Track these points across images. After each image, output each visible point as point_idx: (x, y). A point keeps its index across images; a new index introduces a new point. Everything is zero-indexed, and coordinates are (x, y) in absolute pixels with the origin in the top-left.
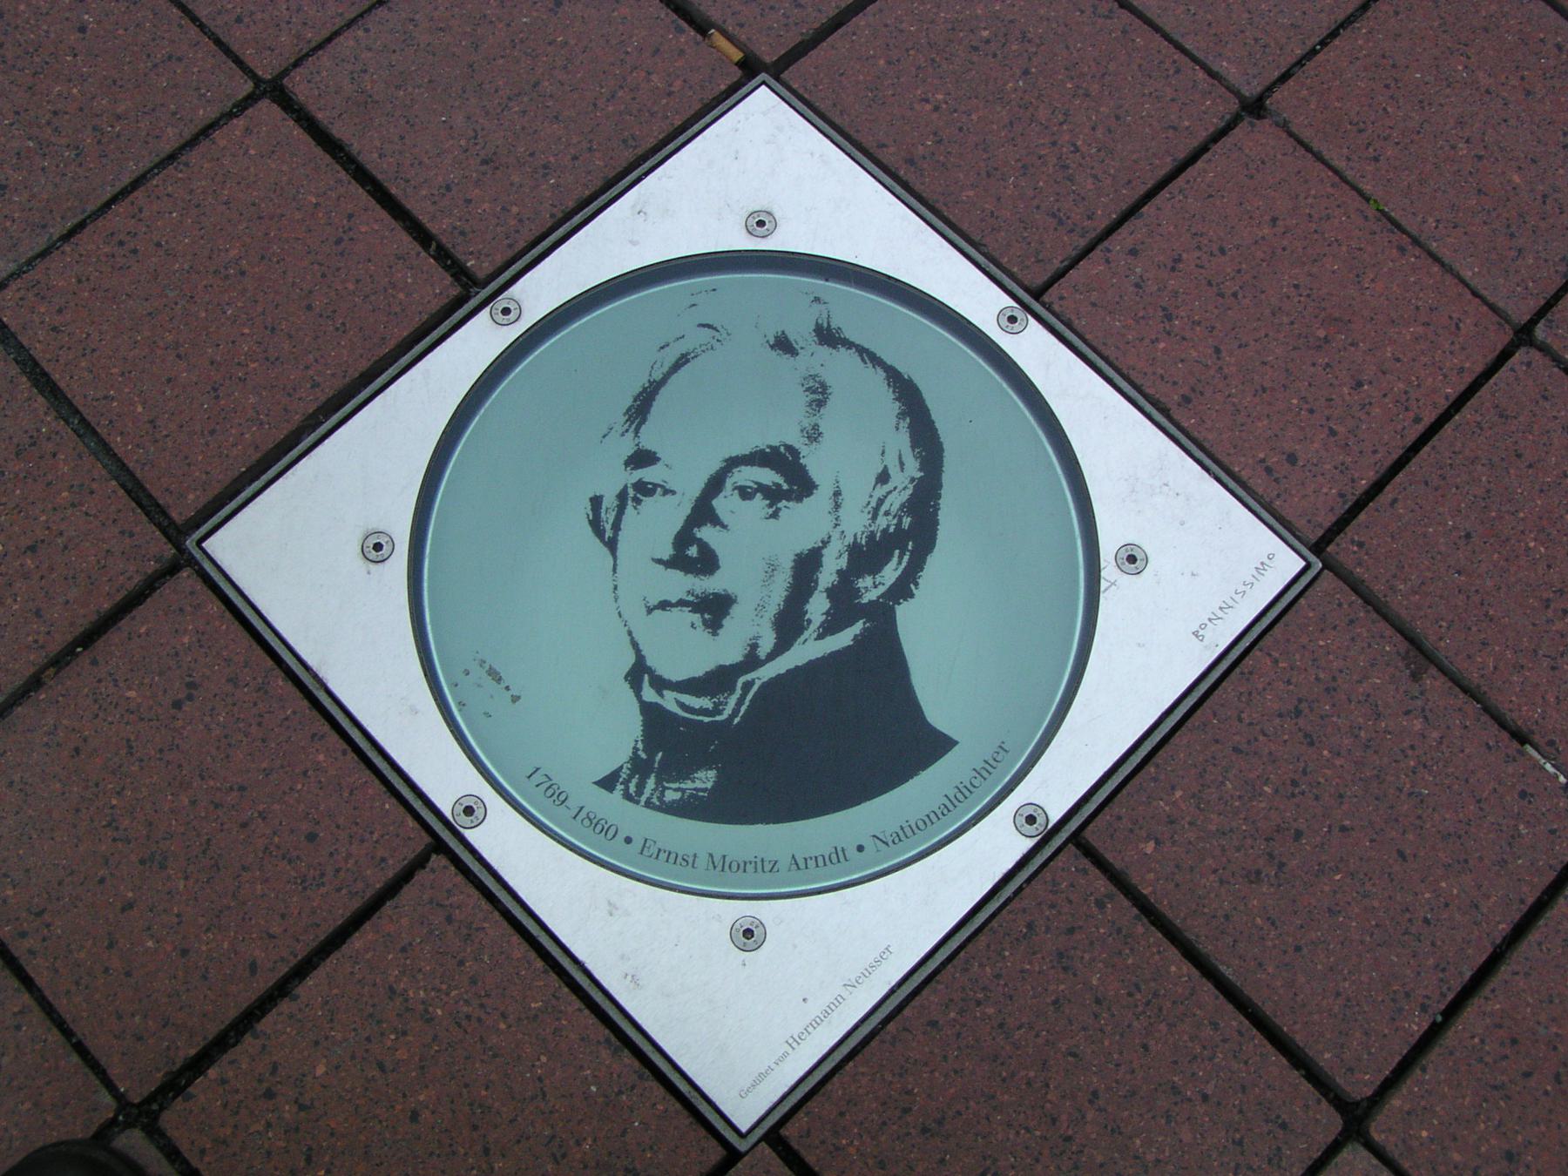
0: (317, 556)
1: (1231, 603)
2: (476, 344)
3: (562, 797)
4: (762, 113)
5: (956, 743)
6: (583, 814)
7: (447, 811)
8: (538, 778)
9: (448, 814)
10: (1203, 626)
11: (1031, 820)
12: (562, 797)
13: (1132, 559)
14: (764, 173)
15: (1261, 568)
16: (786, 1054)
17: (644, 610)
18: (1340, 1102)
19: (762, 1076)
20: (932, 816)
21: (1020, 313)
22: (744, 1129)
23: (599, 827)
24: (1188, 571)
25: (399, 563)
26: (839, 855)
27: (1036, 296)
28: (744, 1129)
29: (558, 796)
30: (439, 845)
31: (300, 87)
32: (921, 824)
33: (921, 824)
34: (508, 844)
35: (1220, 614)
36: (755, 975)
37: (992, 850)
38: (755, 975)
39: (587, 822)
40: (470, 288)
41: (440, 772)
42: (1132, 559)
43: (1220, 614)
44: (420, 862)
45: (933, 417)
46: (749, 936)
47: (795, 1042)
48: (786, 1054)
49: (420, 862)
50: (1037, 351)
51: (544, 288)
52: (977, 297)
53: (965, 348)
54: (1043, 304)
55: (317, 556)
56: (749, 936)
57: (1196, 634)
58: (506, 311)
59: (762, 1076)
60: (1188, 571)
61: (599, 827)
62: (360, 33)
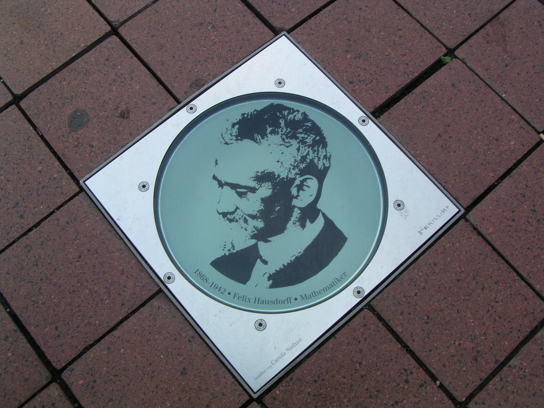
0: (123, 187)
1: (432, 222)
2: (182, 118)
15: (444, 211)
19: (262, 373)
23: (202, 278)
24: (416, 208)
26: (289, 300)
28: (255, 391)
30: (160, 292)
32: (281, 302)
33: (281, 302)
34: (180, 288)
35: (428, 226)
36: (260, 339)
37: (344, 302)
38: (260, 339)
39: (199, 275)
40: (178, 102)
41: (160, 263)
42: (261, 325)
43: (428, 226)
47: (283, 355)
48: (271, 366)
50: (372, 132)
53: (375, 168)
55: (123, 187)
57: (420, 232)
58: (191, 108)
60: (416, 208)
61: (202, 278)
62: (528, 330)
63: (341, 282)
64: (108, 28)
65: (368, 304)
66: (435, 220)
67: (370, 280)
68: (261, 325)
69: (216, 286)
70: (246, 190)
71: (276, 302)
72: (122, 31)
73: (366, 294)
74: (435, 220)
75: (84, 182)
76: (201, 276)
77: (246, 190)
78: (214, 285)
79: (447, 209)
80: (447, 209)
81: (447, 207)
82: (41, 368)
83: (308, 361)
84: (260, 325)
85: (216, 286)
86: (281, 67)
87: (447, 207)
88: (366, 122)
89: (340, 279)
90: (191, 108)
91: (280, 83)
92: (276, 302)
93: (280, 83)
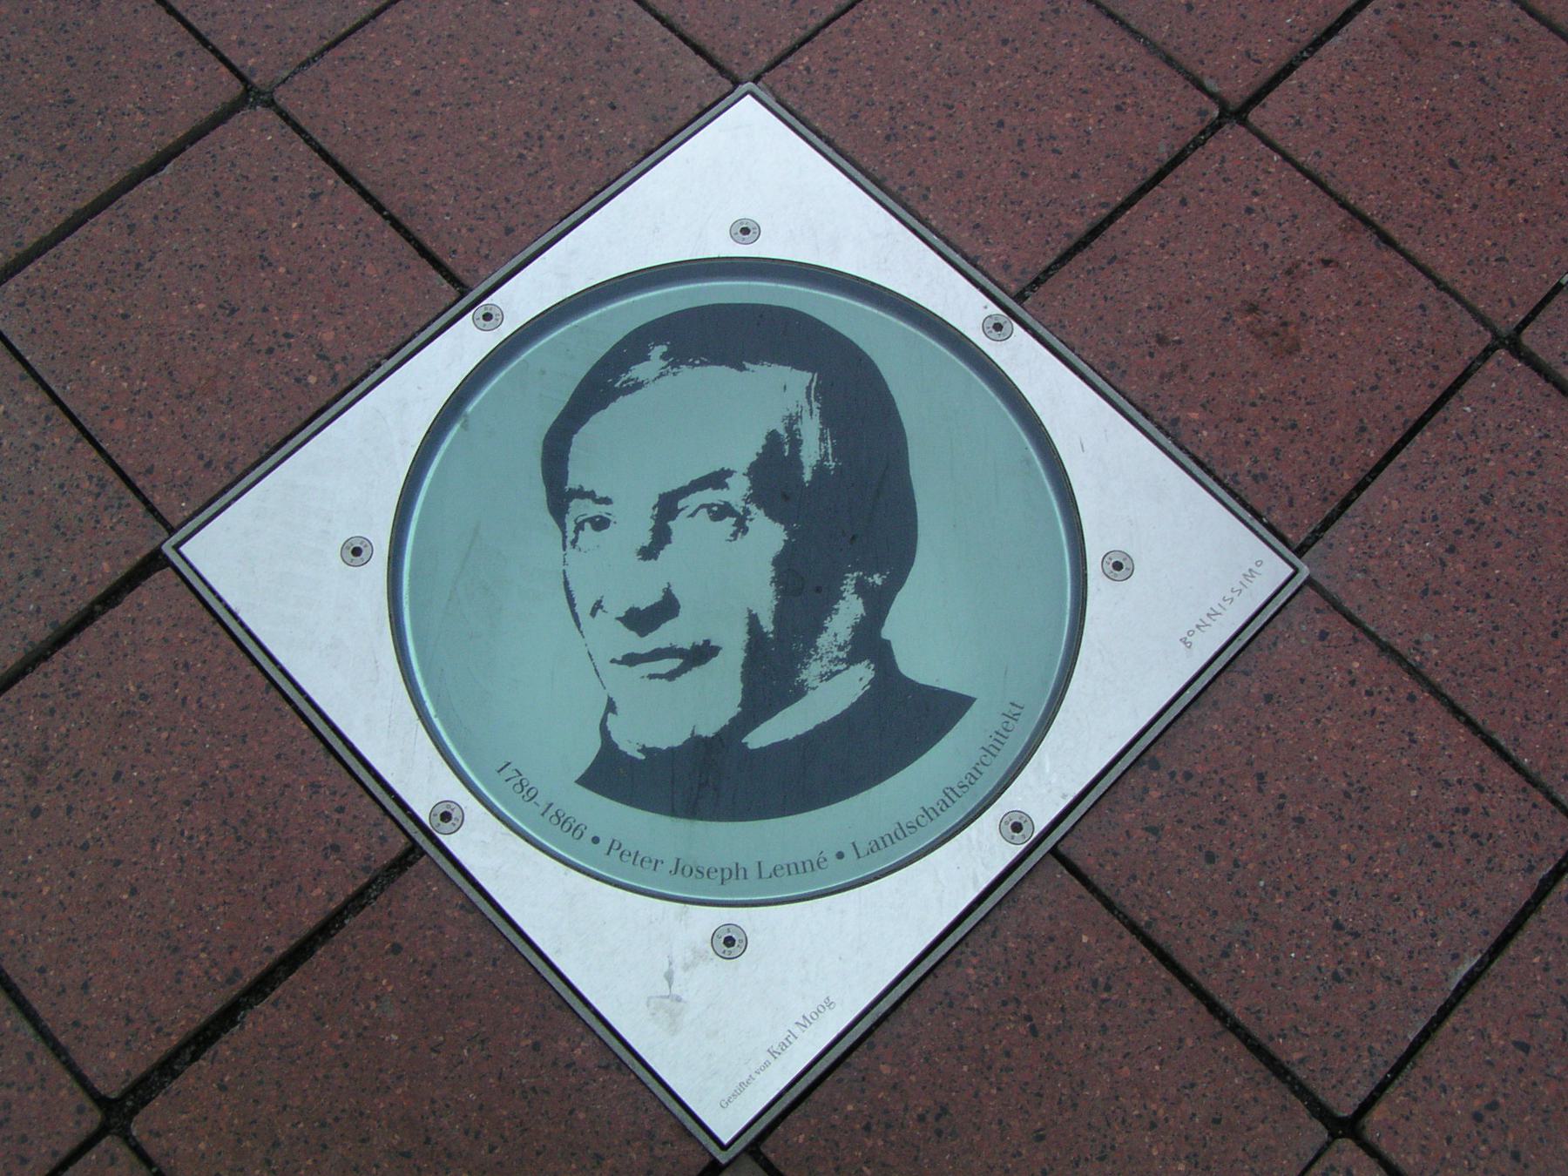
0: (301, 558)
1: (1219, 609)
2: (459, 348)
3: (532, 794)
6: (552, 811)
7: (424, 817)
8: (508, 772)
10: (1190, 633)
12: (532, 794)
14: (743, 186)
16: (767, 1064)
20: (887, 839)
22: (726, 1141)
23: (567, 826)
24: (1168, 575)
25: (378, 566)
27: (1023, 295)
28: (726, 1141)
29: (527, 791)
30: (412, 854)
31: (114, 1068)
34: (486, 851)
35: (1208, 621)
36: (735, 987)
38: (735, 987)
39: (555, 820)
40: (459, 287)
41: (419, 778)
42: (1119, 567)
43: (1208, 621)
44: (164, 523)
45: (810, 727)
48: (767, 1064)
49: (164, 523)
50: (1025, 359)
55: (301, 558)
56: (1119, 567)
57: (1184, 641)
60: (1168, 575)
61: (567, 826)
65: (1054, 851)
67: (1046, 789)
68: (730, 942)
70: (759, 738)
71: (900, 834)
73: (443, 838)
75: (177, 547)
76: (561, 820)
77: (759, 738)
79: (1259, 570)
80: (1259, 570)
83: (197, 1077)
84: (729, 942)
86: (743, 186)
87: (1259, 563)
88: (1006, 327)
90: (487, 317)
91: (745, 231)
92: (900, 834)
93: (745, 231)
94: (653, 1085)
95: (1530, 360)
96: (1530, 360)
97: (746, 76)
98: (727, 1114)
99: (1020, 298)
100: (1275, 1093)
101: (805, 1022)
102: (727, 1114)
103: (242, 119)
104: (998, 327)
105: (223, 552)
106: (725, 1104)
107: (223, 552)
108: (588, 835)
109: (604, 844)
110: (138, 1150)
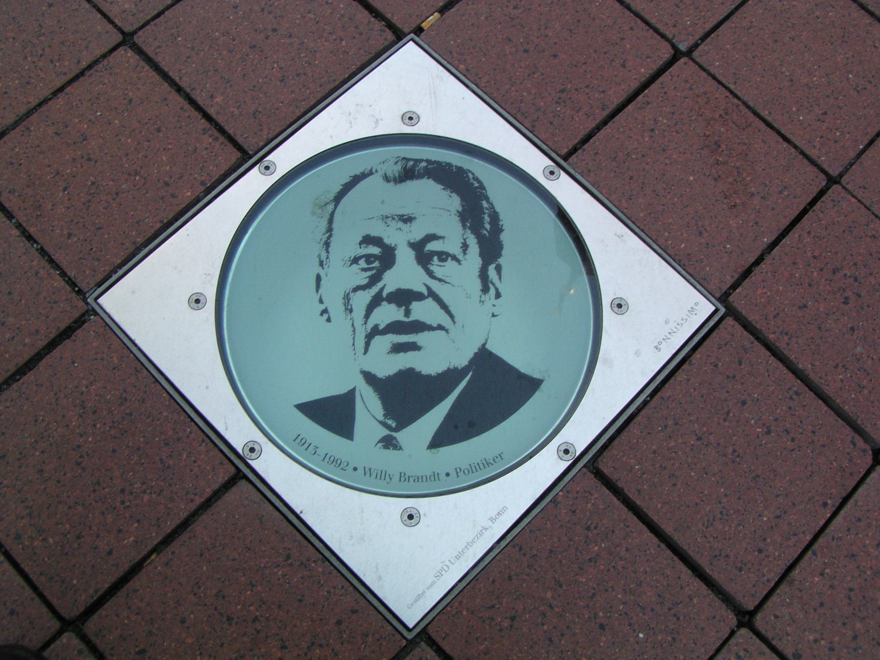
0: (163, 306)
1: (675, 330)
2: (252, 185)
4: (410, 57)
5: (401, 448)
9: (240, 452)
10: (660, 343)
11: (566, 452)
12: (339, 462)
13: (619, 306)
17: (329, 310)
18: (841, 176)
19: (419, 597)
21: (556, 170)
22: (411, 626)
24: (651, 311)
27: (565, 158)
30: (239, 473)
34: (275, 468)
35: (669, 336)
36: (413, 541)
37: (545, 469)
38: (413, 541)
40: (246, 157)
41: (236, 429)
42: (619, 306)
43: (669, 336)
46: (197, 301)
50: (567, 192)
51: (287, 156)
52: (532, 160)
54: (569, 164)
55: (163, 306)
56: (197, 301)
57: (656, 347)
58: (267, 168)
59: (419, 597)
63: (491, 467)
64: (119, 38)
66: (679, 327)
67: (583, 430)
69: (303, 441)
72: (139, 39)
74: (679, 327)
78: (300, 438)
81: (696, 304)
82: (84, 599)
85: (303, 441)
86: (410, 92)
87: (696, 304)
89: (492, 461)
90: (267, 168)
93: (410, 118)
94: (444, 603)
95: (140, 52)
96: (140, 52)
97: (406, 30)
98: (411, 613)
99: (565, 158)
100: (768, 260)
101: (469, 545)
102: (411, 613)
103: (121, 51)
104: (552, 173)
105: (121, 302)
106: (410, 606)
107: (121, 302)
108: (361, 471)
109: (443, 476)
110: (732, 633)
